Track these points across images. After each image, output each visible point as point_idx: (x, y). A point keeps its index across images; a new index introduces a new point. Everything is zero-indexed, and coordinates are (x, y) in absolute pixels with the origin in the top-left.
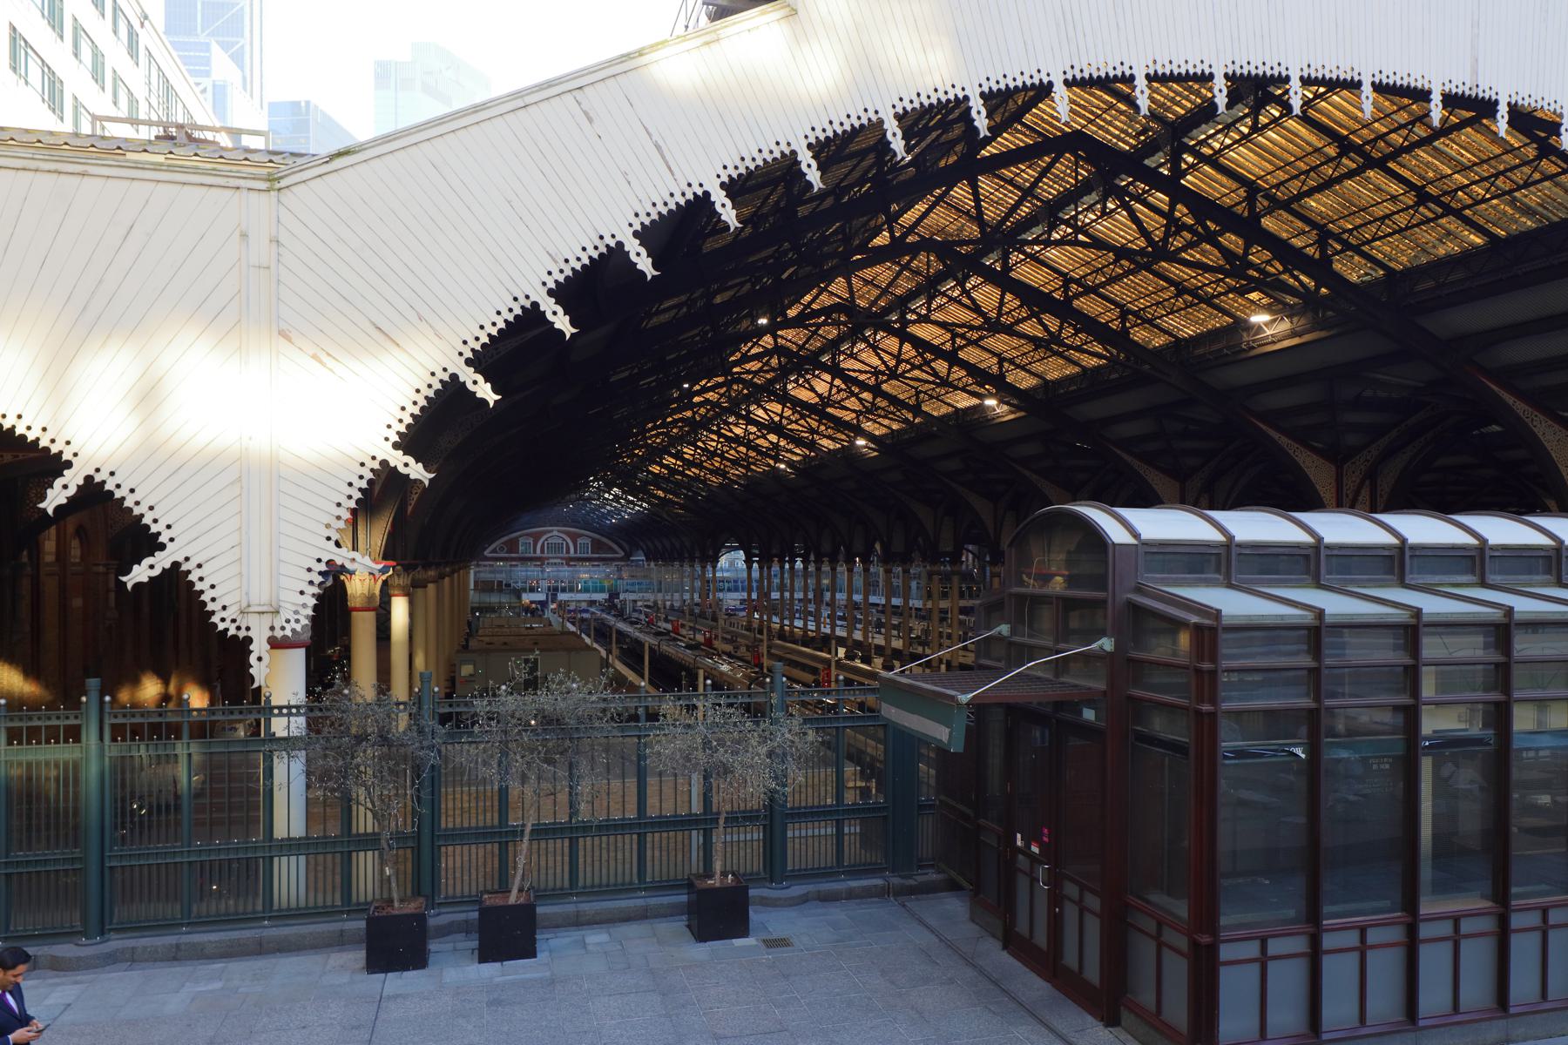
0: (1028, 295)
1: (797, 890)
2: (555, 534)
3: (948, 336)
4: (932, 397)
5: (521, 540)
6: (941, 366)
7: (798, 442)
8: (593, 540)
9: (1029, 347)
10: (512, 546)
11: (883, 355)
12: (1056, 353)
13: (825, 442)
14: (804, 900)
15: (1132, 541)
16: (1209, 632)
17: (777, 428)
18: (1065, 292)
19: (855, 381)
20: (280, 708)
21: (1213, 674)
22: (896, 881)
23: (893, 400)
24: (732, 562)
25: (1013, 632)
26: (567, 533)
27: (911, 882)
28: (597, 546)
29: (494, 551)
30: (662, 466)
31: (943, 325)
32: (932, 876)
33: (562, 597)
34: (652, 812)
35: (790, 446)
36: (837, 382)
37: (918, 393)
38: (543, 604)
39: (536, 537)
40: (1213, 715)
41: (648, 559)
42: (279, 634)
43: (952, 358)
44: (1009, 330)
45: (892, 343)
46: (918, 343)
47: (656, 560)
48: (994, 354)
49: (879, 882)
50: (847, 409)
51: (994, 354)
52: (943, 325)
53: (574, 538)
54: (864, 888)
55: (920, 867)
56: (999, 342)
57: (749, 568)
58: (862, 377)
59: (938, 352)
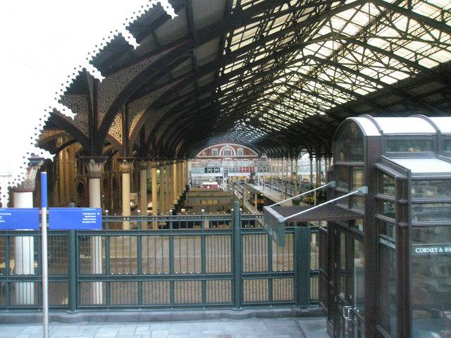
0: (423, 20)
1: (247, 312)
2: (227, 147)
3: (389, 44)
4: (385, 75)
5: (213, 150)
6: (385, 60)
7: (327, 100)
8: (244, 149)
9: (430, 46)
10: (209, 152)
11: (355, 54)
12: (442, 49)
13: (339, 99)
14: (249, 316)
15: (380, 135)
16: (405, 183)
17: (315, 94)
18: (442, 17)
19: (348, 70)
20: (126, 218)
21: (406, 205)
22: (298, 309)
23: (367, 77)
24: (305, 157)
25: (337, 185)
26: (233, 146)
27: (306, 310)
28: (246, 152)
29: (201, 155)
30: (269, 114)
31: (384, 38)
32: (316, 308)
33: (230, 175)
34: (275, 269)
35: (323, 102)
36: (338, 70)
37: (378, 73)
38: (221, 178)
39: (219, 148)
40: (407, 228)
41: (268, 157)
42: (12, 185)
43: (390, 54)
44: (417, 39)
45: (360, 49)
46: (373, 49)
47: (271, 157)
48: (413, 51)
49: (289, 310)
50: (347, 83)
51: (413, 51)
52: (384, 38)
53: (236, 148)
54: (283, 312)
55: (312, 304)
56: (415, 45)
57: (311, 160)
58: (351, 67)
59: (384, 52)
